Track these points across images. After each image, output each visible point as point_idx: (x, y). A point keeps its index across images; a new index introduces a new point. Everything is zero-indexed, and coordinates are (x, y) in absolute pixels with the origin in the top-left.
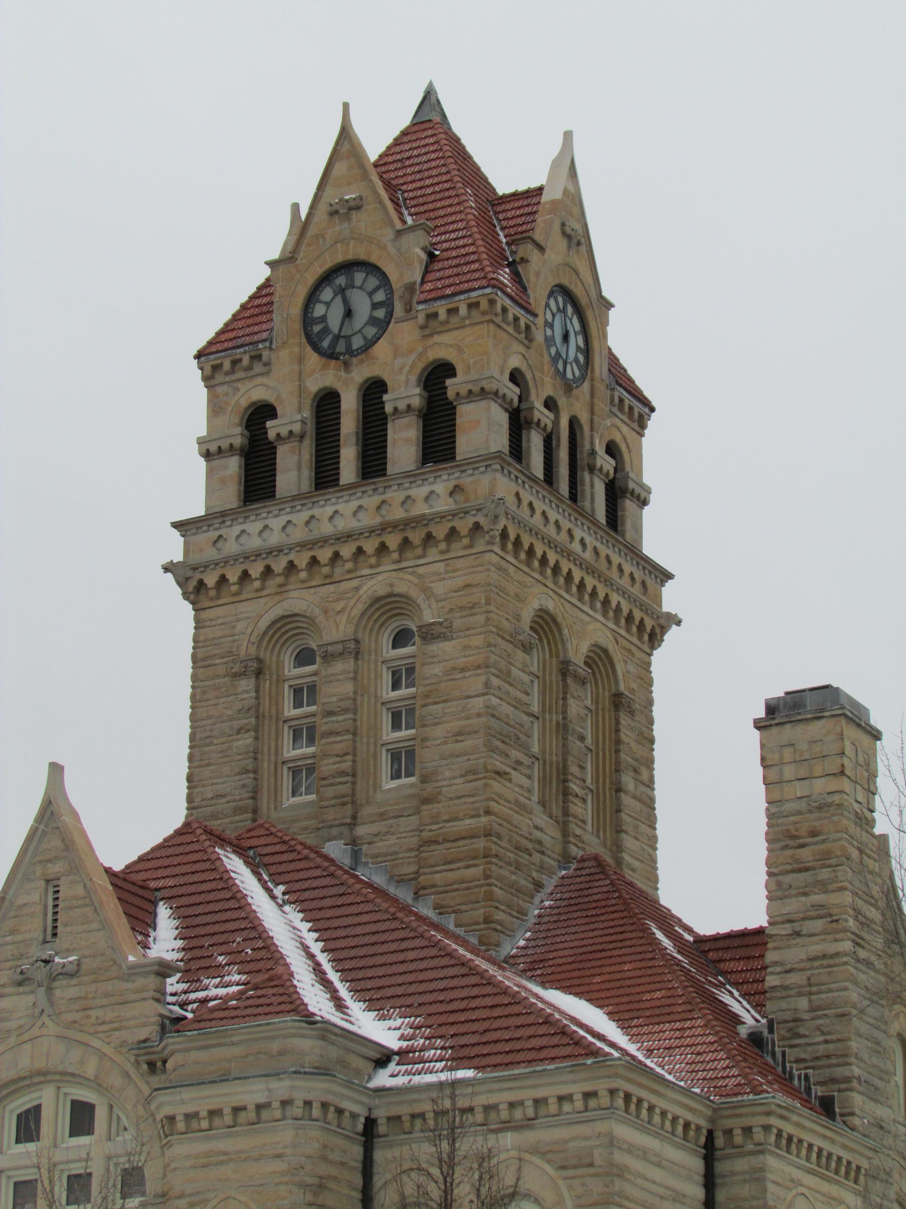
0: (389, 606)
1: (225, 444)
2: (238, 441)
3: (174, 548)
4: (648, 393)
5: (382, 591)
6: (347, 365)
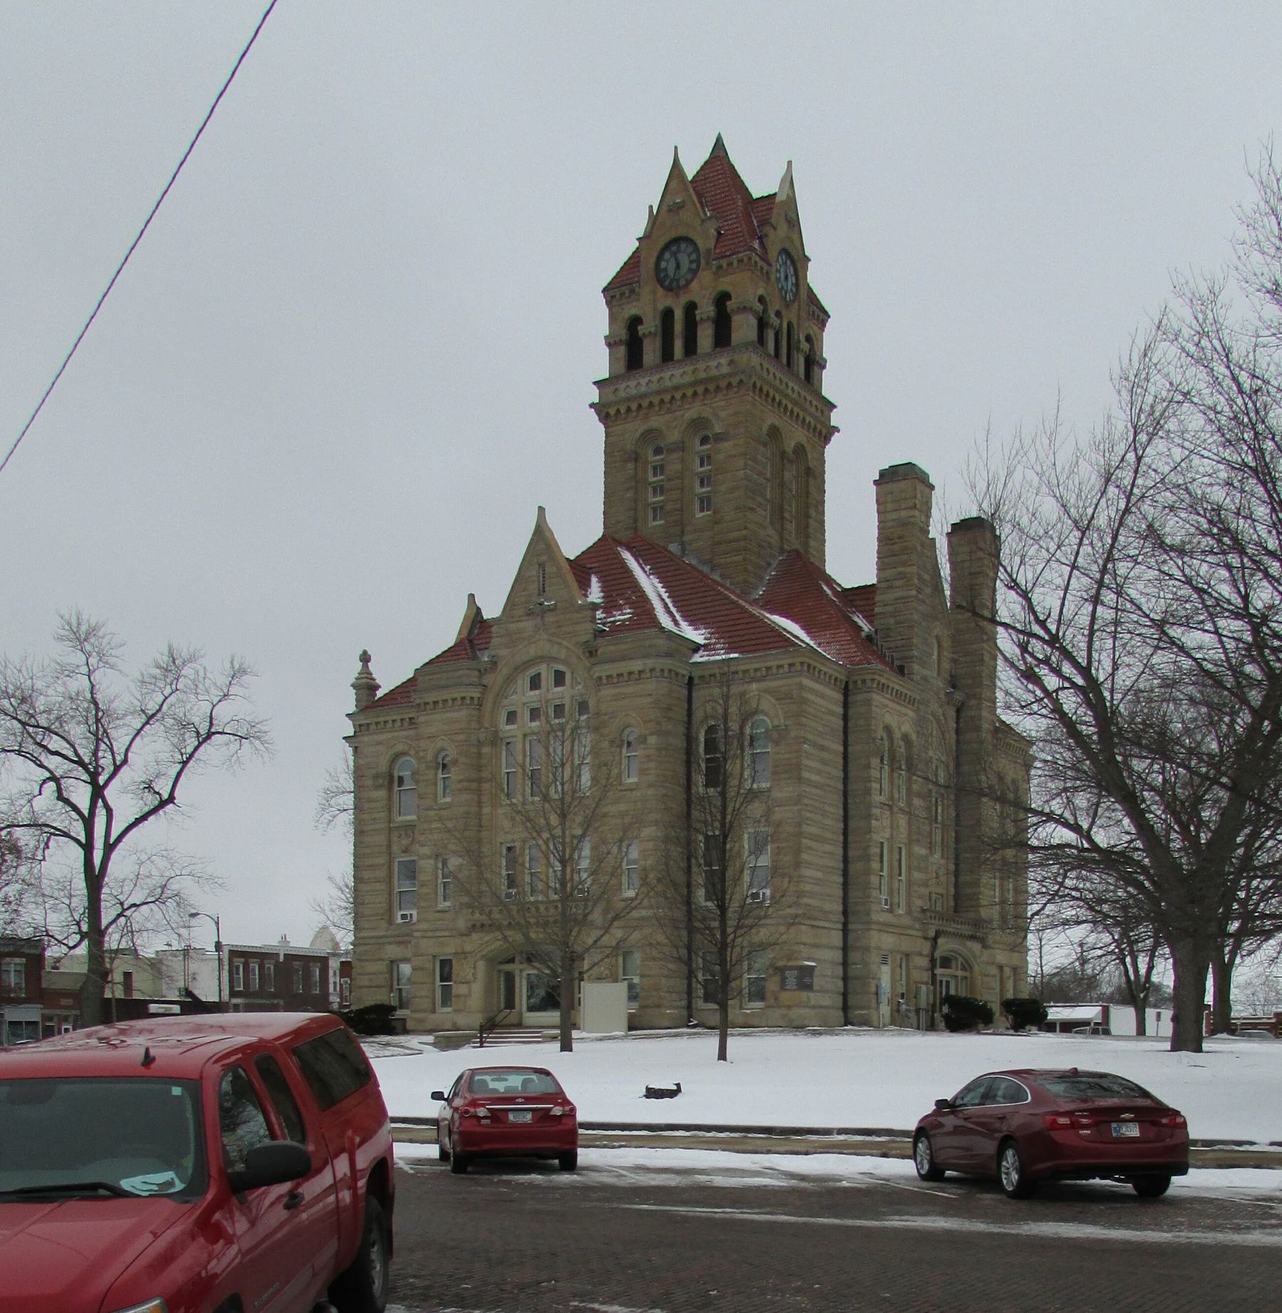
0: (699, 424)
5: (695, 416)
6: (677, 295)
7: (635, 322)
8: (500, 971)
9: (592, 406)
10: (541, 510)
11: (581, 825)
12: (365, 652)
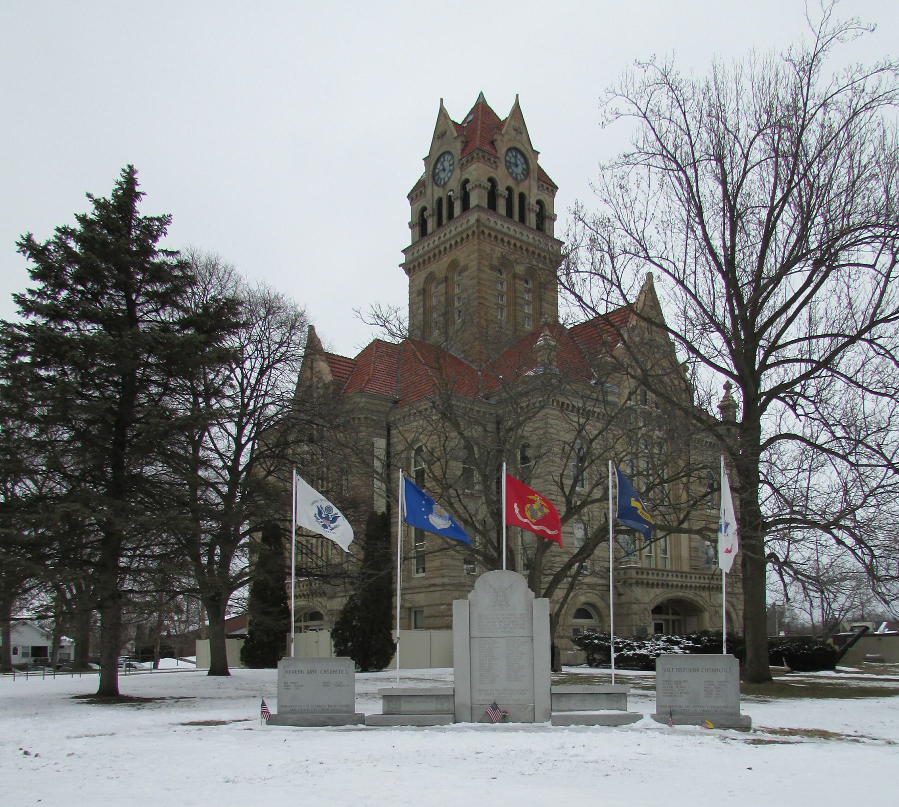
4: (556, 184)
11: (696, 216)
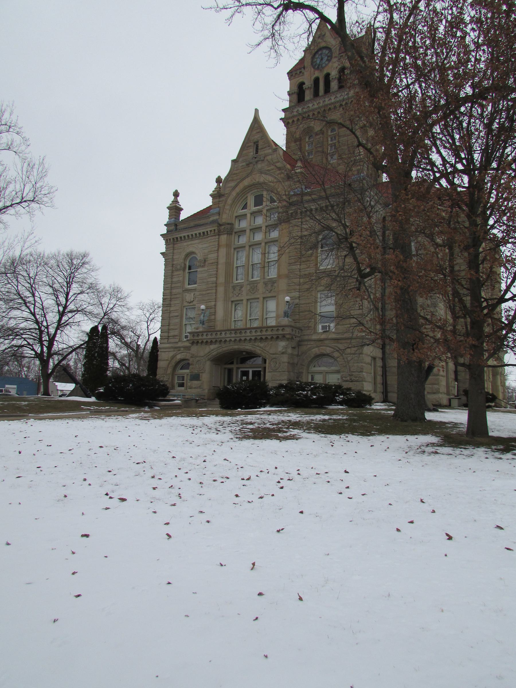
1: (293, 92)
2: (296, 91)
3: (283, 115)
7: (302, 84)
8: (225, 368)
9: (281, 119)
10: (257, 111)
12: (176, 191)
